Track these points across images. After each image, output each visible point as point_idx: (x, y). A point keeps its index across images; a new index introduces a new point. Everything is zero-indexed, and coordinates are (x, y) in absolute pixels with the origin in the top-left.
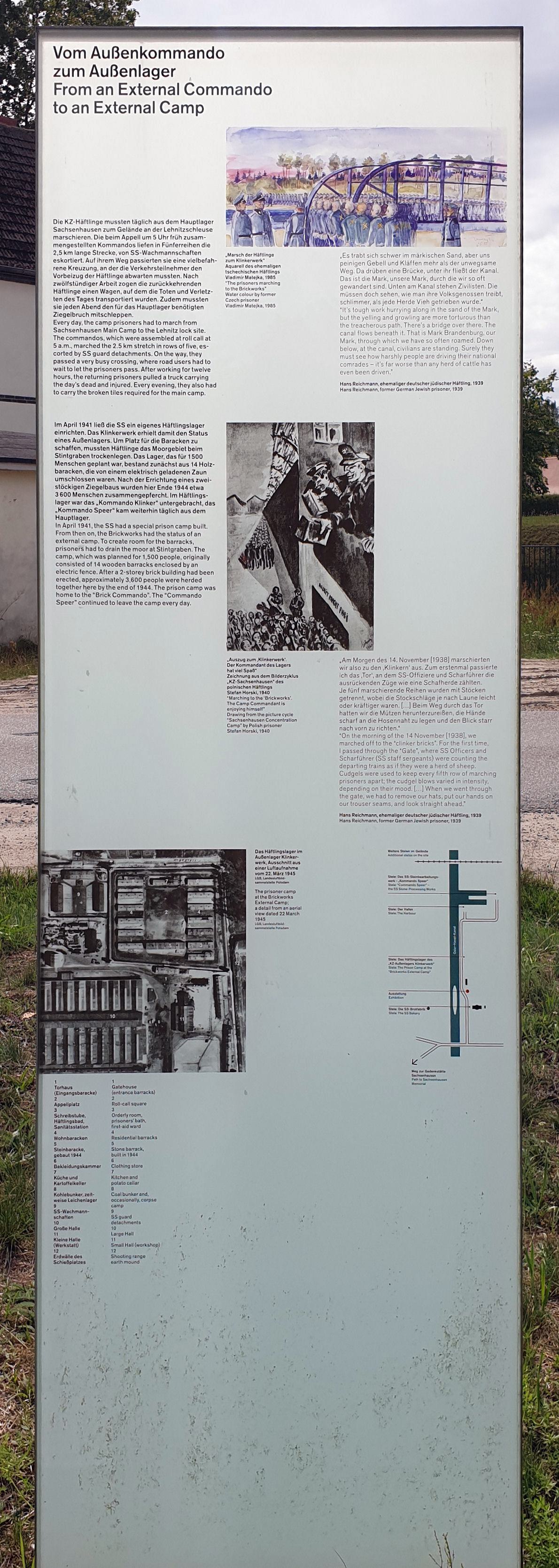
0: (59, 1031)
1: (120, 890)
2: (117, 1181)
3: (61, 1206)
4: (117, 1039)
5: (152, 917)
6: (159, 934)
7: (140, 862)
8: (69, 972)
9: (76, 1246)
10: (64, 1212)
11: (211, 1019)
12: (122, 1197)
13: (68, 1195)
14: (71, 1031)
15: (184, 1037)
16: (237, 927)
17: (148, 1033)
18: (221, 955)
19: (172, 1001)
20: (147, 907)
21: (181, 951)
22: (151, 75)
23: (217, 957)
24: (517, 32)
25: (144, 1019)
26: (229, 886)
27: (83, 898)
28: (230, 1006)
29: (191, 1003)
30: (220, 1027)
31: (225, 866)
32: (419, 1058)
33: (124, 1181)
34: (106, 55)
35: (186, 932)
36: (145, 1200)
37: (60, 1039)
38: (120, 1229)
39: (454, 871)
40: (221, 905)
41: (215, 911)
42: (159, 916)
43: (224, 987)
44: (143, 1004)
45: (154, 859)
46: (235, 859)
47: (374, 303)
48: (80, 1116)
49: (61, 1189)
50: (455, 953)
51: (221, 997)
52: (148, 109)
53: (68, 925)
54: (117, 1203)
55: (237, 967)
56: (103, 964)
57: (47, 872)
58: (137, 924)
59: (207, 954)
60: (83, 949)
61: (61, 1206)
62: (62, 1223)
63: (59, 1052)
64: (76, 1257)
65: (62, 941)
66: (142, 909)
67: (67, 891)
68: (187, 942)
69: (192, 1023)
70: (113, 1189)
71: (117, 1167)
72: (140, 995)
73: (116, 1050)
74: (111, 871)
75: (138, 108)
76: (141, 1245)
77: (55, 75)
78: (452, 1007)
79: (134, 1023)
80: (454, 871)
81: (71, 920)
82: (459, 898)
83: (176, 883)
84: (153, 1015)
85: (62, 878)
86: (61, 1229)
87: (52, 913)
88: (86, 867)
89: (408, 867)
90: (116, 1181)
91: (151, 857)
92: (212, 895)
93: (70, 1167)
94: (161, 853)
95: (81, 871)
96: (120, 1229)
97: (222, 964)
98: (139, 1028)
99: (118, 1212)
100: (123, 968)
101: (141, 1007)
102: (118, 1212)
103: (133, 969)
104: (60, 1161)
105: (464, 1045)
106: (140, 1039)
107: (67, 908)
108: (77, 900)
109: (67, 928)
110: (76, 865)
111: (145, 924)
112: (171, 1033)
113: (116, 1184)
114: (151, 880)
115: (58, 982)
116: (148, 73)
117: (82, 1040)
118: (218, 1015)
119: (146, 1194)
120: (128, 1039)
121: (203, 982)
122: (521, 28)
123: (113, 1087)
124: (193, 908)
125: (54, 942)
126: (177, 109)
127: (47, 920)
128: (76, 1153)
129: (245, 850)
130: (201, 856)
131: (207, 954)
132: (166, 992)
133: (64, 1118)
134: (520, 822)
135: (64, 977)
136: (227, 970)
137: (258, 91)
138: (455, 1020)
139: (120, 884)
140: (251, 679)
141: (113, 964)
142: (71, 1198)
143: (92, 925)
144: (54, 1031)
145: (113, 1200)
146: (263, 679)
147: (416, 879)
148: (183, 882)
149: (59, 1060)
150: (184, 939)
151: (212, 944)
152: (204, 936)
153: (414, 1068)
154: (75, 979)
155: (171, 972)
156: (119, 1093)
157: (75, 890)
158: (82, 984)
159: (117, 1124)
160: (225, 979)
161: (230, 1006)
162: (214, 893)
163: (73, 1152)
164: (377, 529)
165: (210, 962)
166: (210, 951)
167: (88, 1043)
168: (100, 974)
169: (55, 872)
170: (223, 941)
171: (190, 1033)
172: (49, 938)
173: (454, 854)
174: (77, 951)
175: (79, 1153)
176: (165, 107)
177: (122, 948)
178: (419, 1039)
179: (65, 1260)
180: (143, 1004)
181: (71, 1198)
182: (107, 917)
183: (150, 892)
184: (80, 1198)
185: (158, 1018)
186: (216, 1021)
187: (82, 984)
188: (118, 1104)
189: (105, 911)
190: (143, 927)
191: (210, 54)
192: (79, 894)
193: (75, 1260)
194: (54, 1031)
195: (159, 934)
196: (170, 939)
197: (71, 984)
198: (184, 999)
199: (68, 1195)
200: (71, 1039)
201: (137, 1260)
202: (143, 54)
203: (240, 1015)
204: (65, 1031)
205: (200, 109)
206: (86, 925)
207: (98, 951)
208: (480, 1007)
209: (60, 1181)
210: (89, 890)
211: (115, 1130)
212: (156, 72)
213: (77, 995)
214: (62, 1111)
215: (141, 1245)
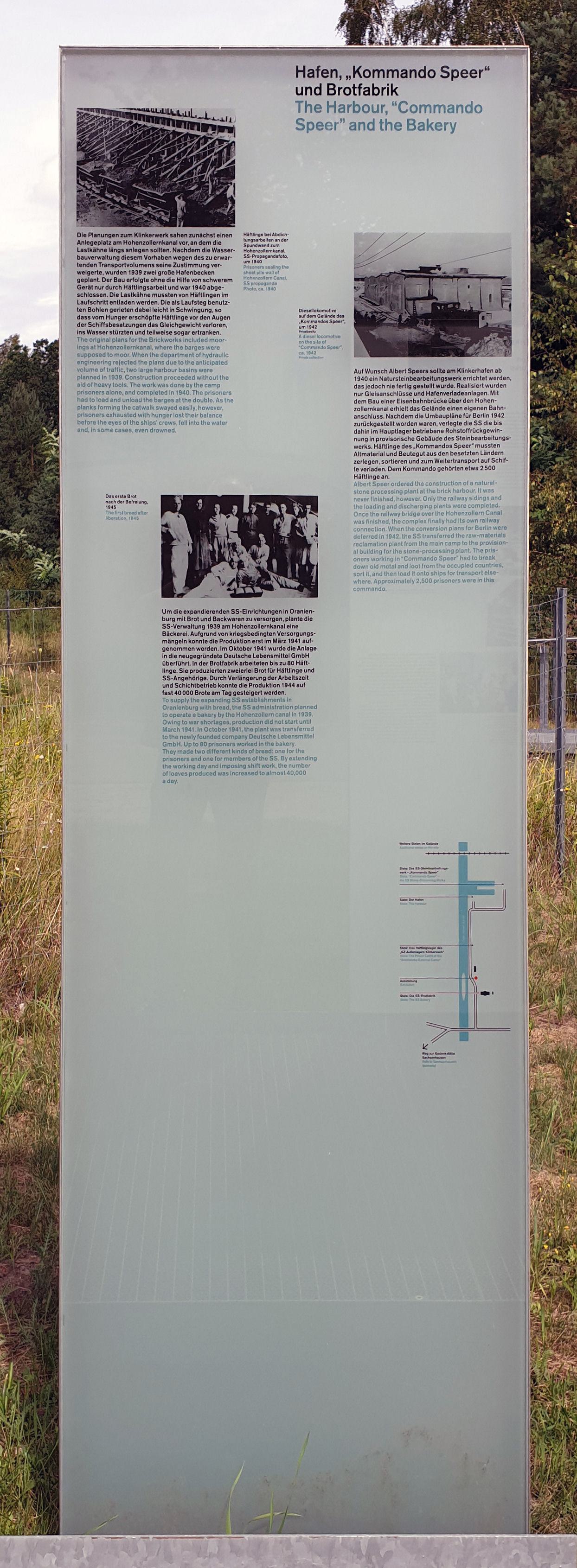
32: (430, 1043)
82: (468, 888)
89: (418, 858)
105: (472, 1030)
137: (469, 109)
147: (427, 871)
153: (424, 1051)
164: (160, 535)
178: (430, 1024)
191: (422, 74)
202: (430, 126)
208: (488, 993)
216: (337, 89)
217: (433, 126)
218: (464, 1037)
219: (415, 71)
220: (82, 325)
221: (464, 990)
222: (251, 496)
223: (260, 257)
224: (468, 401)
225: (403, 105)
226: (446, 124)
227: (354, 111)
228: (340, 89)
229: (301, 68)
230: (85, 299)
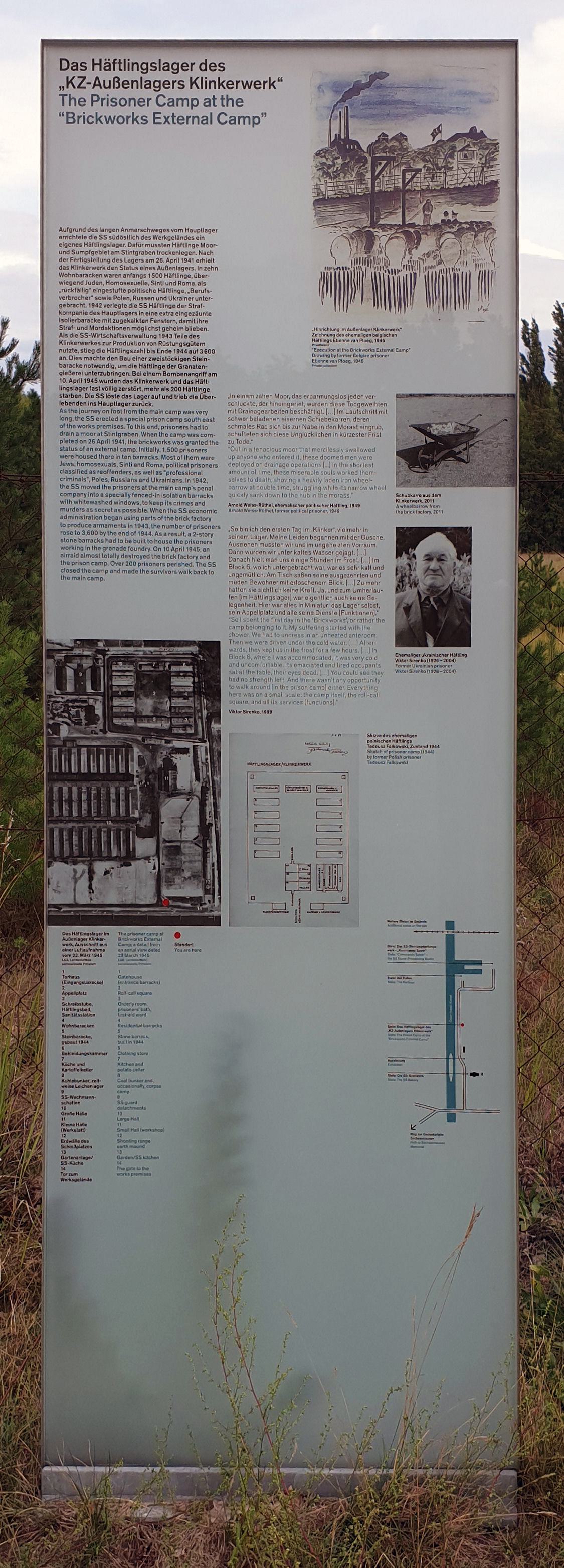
0: (65, 789)
1: (114, 674)
2: (123, 1067)
3: (68, 1092)
4: (113, 796)
5: (142, 696)
6: (148, 711)
7: (131, 650)
8: (73, 740)
9: (83, 1130)
10: (72, 1097)
11: (191, 782)
12: (127, 1083)
13: (75, 1081)
14: (75, 789)
15: (169, 796)
16: (213, 706)
17: (139, 793)
18: (200, 729)
19: (159, 766)
20: (136, 687)
21: (166, 726)
23: (196, 730)
25: (136, 780)
26: (206, 671)
27: (83, 679)
28: (207, 771)
29: (175, 768)
30: (199, 788)
31: (203, 655)
33: (130, 1067)
34: (107, 85)
35: (170, 710)
36: (151, 1086)
37: (66, 795)
38: (127, 1114)
39: (450, 942)
40: (200, 688)
41: (194, 692)
42: (147, 696)
43: (202, 756)
44: (134, 768)
45: (143, 648)
46: (211, 649)
48: (87, 1004)
49: (68, 1075)
50: (451, 1021)
51: (200, 764)
52: (206, 120)
53: (71, 702)
54: (123, 1089)
55: (214, 739)
56: (101, 735)
57: (53, 657)
58: (129, 702)
59: (188, 728)
60: (84, 722)
61: (68, 1092)
62: (70, 1108)
63: (65, 806)
64: (83, 1141)
65: (66, 715)
66: (133, 690)
67: (70, 673)
68: (171, 718)
69: (176, 785)
70: (119, 1075)
71: (123, 1054)
72: (132, 761)
73: (113, 805)
74: (107, 657)
75: (196, 119)
76: (147, 1130)
78: (448, 1073)
79: (128, 784)
80: (450, 942)
81: (74, 697)
82: (454, 967)
83: (161, 669)
84: (143, 777)
85: (66, 662)
86: (68, 1114)
87: (58, 692)
88: (86, 653)
89: (406, 936)
90: (122, 1067)
91: (140, 646)
92: (191, 679)
93: (77, 1054)
94: (148, 643)
95: (81, 656)
96: (127, 1114)
97: (200, 736)
98: (131, 788)
99: (124, 1097)
100: (117, 738)
101: (133, 771)
102: (124, 1097)
103: (126, 739)
104: (68, 1048)
106: (133, 797)
107: (70, 688)
108: (79, 680)
109: (70, 704)
110: (77, 651)
111: (136, 702)
112: (159, 793)
113: (122, 1070)
114: (141, 666)
115: (63, 749)
117: (84, 796)
118: (198, 779)
119: (151, 1081)
120: (122, 797)
121: (185, 751)
123: (120, 977)
124: (176, 690)
125: (60, 716)
127: (53, 697)
128: (83, 1040)
129: (218, 643)
130: (182, 646)
131: (188, 728)
132: (154, 759)
133: (72, 1007)
135: (68, 744)
136: (205, 742)
138: (451, 1087)
139: (114, 668)
141: (110, 735)
142: (78, 1084)
143: (91, 702)
144: (60, 789)
145: (119, 1086)
148: (167, 668)
149: (65, 813)
150: (169, 716)
151: (192, 720)
152: (186, 713)
154: (78, 746)
155: (158, 742)
156: (126, 983)
157: (76, 672)
158: (84, 750)
159: (124, 1013)
160: (203, 749)
161: (207, 771)
162: (193, 677)
163: (80, 1040)
165: (191, 735)
166: (190, 726)
167: (89, 800)
168: (98, 743)
169: (60, 656)
170: (201, 718)
171: (175, 792)
172: (55, 712)
173: (450, 925)
174: (80, 724)
175: (86, 1040)
176: (223, 118)
177: (116, 721)
178: (417, 1104)
179: (72, 1144)
180: (134, 768)
181: (78, 1084)
182: (103, 695)
183: (139, 675)
184: (87, 1084)
185: (147, 780)
186: (195, 783)
187: (84, 750)
188: (125, 993)
189: (102, 691)
190: (134, 705)
192: (81, 674)
193: (82, 1144)
194: (60, 789)
195: (148, 711)
196: (157, 714)
197: (74, 751)
198: (170, 765)
199: (75, 1081)
200: (75, 796)
201: (142, 1144)
202: (220, 84)
203: (215, 778)
204: (70, 790)
205: (256, 120)
206: (86, 702)
207: (96, 724)
209: (67, 1067)
210: (89, 672)
211: (121, 1018)
213: (79, 760)
214: (70, 999)
215: (147, 1130)
216: (76, 117)
217: (225, 84)
218: (451, 1118)
221: (451, 1071)
222: (398, 485)
226: (237, 82)
228: (79, 117)
229: (97, 61)
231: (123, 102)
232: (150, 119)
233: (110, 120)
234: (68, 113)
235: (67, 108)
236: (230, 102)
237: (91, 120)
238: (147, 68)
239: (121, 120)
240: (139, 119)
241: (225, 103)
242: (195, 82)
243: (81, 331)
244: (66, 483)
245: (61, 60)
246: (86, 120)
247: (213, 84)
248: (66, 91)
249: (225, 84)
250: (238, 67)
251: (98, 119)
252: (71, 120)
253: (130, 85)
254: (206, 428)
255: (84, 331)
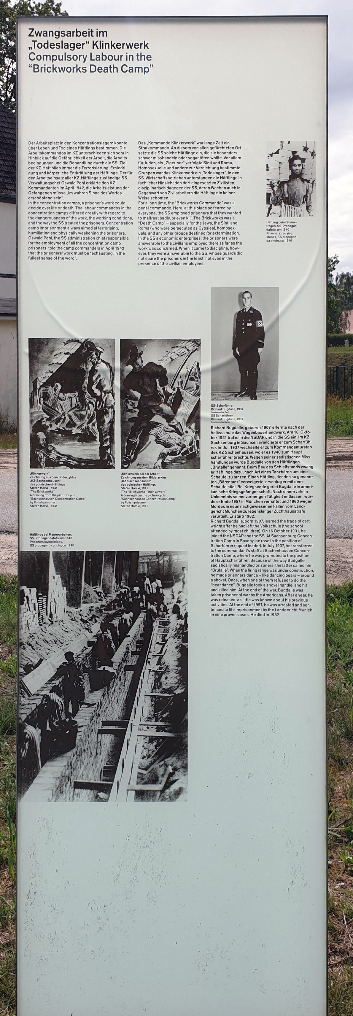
22: (69, 48)
24: (324, 19)
47: (232, 244)
77: (30, 35)
116: (67, 46)
122: (327, 16)
126: (132, 70)
134: (18, 463)
140: (46, 479)
146: (53, 479)
176: (125, 69)
202: (112, 46)
205: (147, 70)
212: (72, 46)
216: (40, 68)
217: (115, 45)
219: (52, 32)
220: (32, 168)
223: (288, 226)
224: (105, 183)
225: (32, 55)
226: (123, 44)
227: (77, 36)
228: (42, 68)
230: (33, 161)
231: (75, 58)
232: (88, 69)
233: (62, 70)
234: (34, 65)
235: (33, 63)
236: (143, 57)
237: (49, 70)
238: (59, 35)
239: (69, 70)
240: (81, 69)
241: (139, 58)
242: (96, 44)
243: (150, 235)
244: (32, 216)
245: (91, 65)
246: (46, 70)
247: (107, 45)
248: (33, 50)
249: (115, 45)
250: (116, 33)
251: (54, 69)
252: (36, 70)
253: (122, 47)
254: (124, 213)
255: (153, 236)
